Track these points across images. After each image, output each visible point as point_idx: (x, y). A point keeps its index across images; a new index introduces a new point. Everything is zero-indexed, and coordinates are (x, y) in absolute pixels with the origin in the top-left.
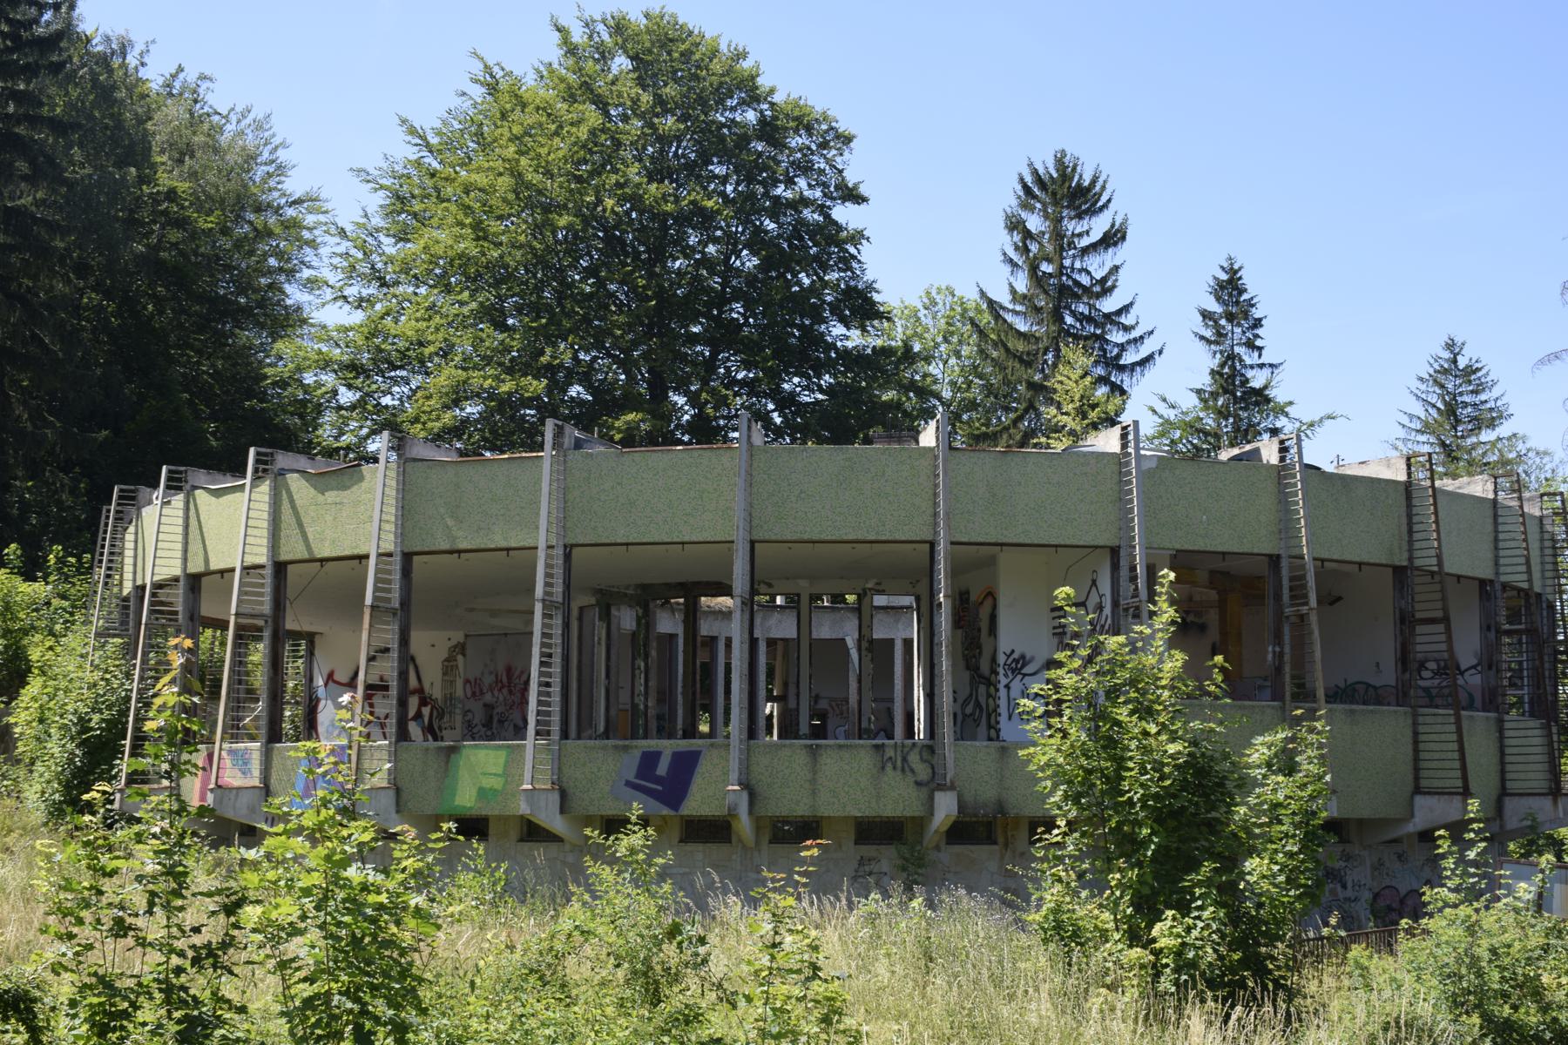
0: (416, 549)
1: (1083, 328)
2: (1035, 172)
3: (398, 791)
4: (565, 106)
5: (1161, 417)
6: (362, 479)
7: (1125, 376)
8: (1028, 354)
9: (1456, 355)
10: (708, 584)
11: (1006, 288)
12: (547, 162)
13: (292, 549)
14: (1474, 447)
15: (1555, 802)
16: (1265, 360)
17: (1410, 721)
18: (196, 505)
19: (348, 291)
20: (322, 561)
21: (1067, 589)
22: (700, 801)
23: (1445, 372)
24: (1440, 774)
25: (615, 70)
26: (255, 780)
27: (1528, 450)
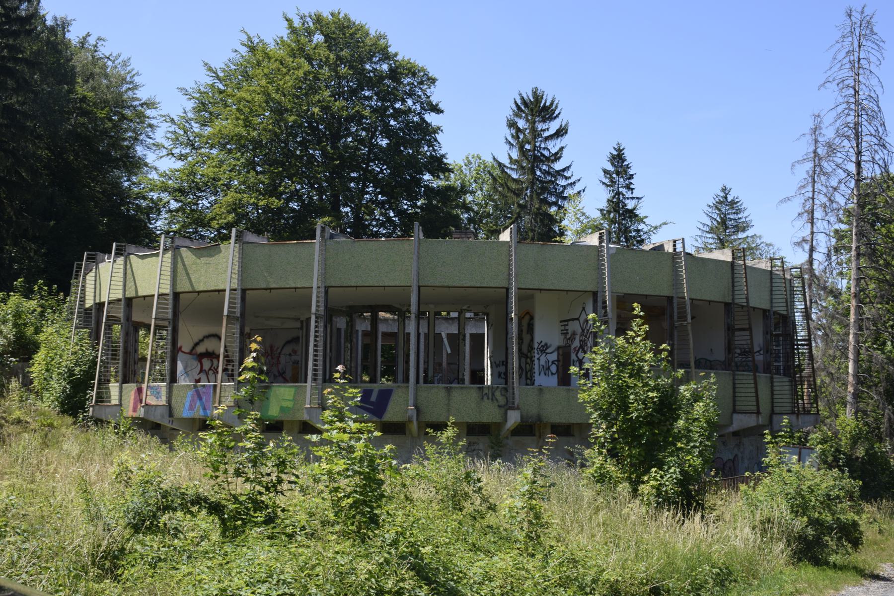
0: (249, 287)
1: (546, 178)
2: (522, 98)
4: (291, 60)
6: (220, 251)
8: (518, 190)
9: (726, 194)
11: (507, 157)
12: (283, 88)
13: (183, 286)
14: (735, 240)
15: (758, 417)
16: (634, 195)
17: (731, 378)
18: (130, 263)
19: (175, 151)
20: (199, 292)
22: (392, 414)
23: (721, 203)
24: (745, 403)
25: (315, 41)
26: (163, 401)
27: (762, 243)
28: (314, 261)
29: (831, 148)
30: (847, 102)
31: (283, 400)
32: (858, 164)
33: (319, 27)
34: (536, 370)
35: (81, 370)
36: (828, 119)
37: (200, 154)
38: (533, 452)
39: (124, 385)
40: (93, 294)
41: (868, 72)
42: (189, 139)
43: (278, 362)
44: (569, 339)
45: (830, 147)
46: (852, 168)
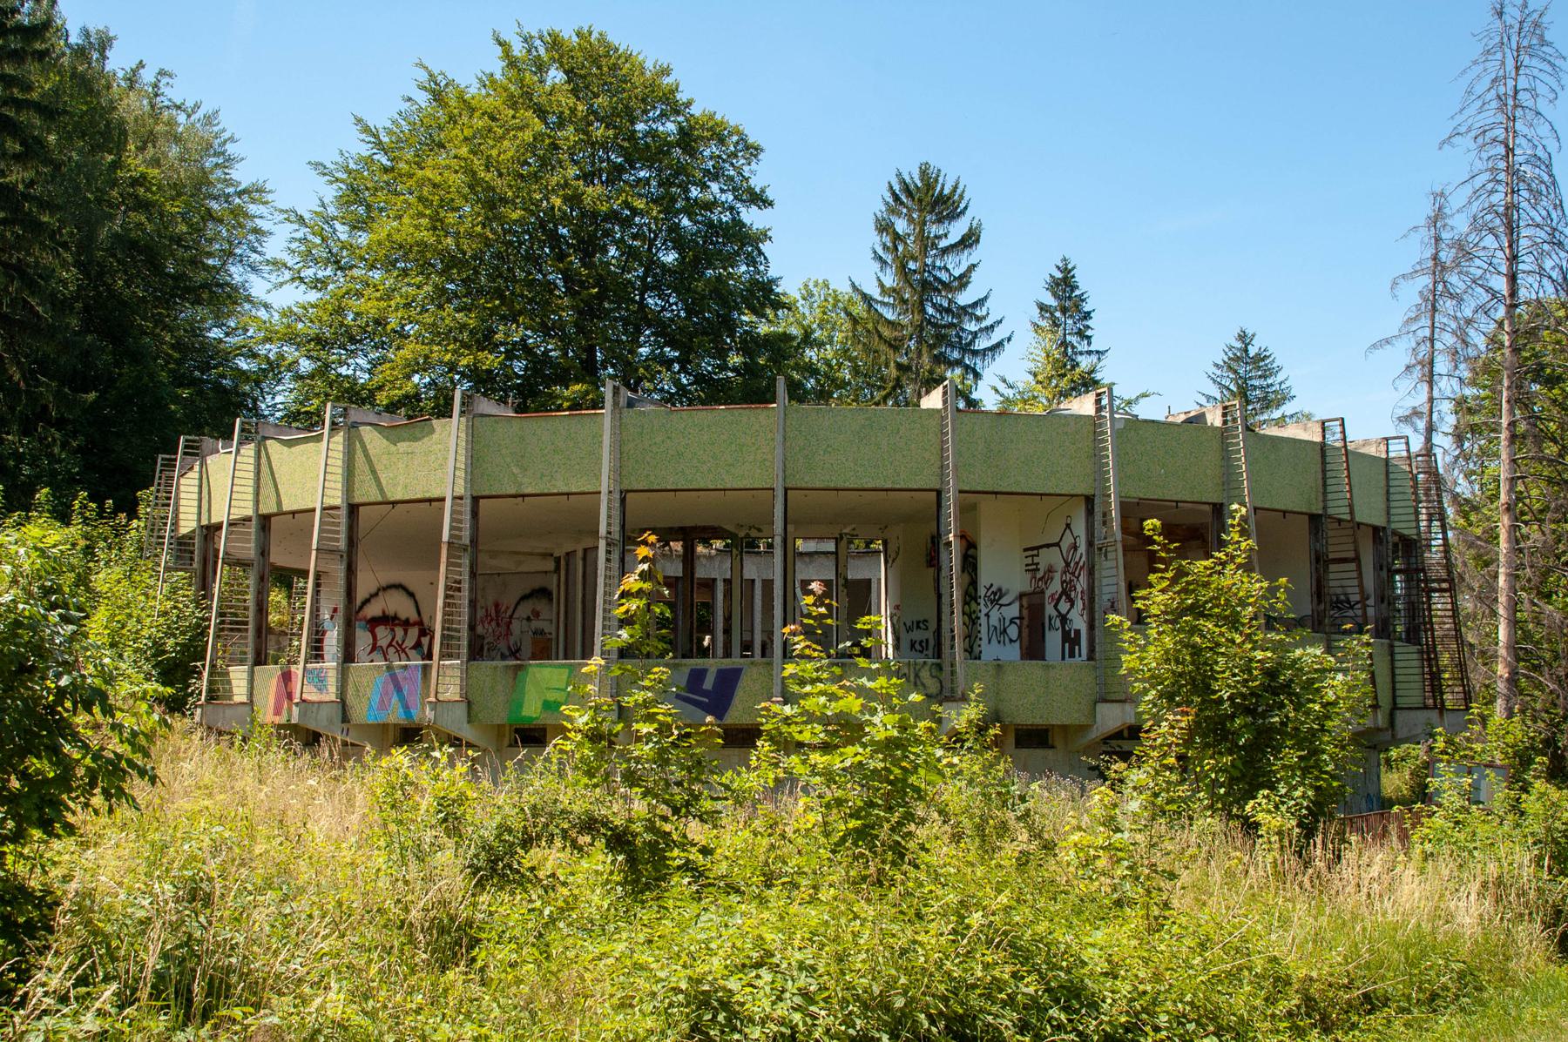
0: (484, 494)
2: (903, 182)
3: (469, 703)
4: (511, 112)
5: (1002, 395)
6: (432, 431)
8: (895, 340)
10: (704, 529)
13: (366, 492)
16: (1092, 348)
18: (267, 454)
20: (394, 503)
21: (1155, 521)
23: (1237, 359)
26: (331, 694)
28: (601, 447)
29: (1464, 251)
30: (1493, 170)
31: (548, 689)
32: (1512, 278)
33: (556, 56)
35: (177, 644)
36: (1457, 200)
37: (353, 278)
39: (257, 668)
40: (195, 510)
41: (1530, 115)
42: (330, 252)
43: (509, 632)
44: (1040, 579)
45: (1461, 248)
46: (1501, 284)
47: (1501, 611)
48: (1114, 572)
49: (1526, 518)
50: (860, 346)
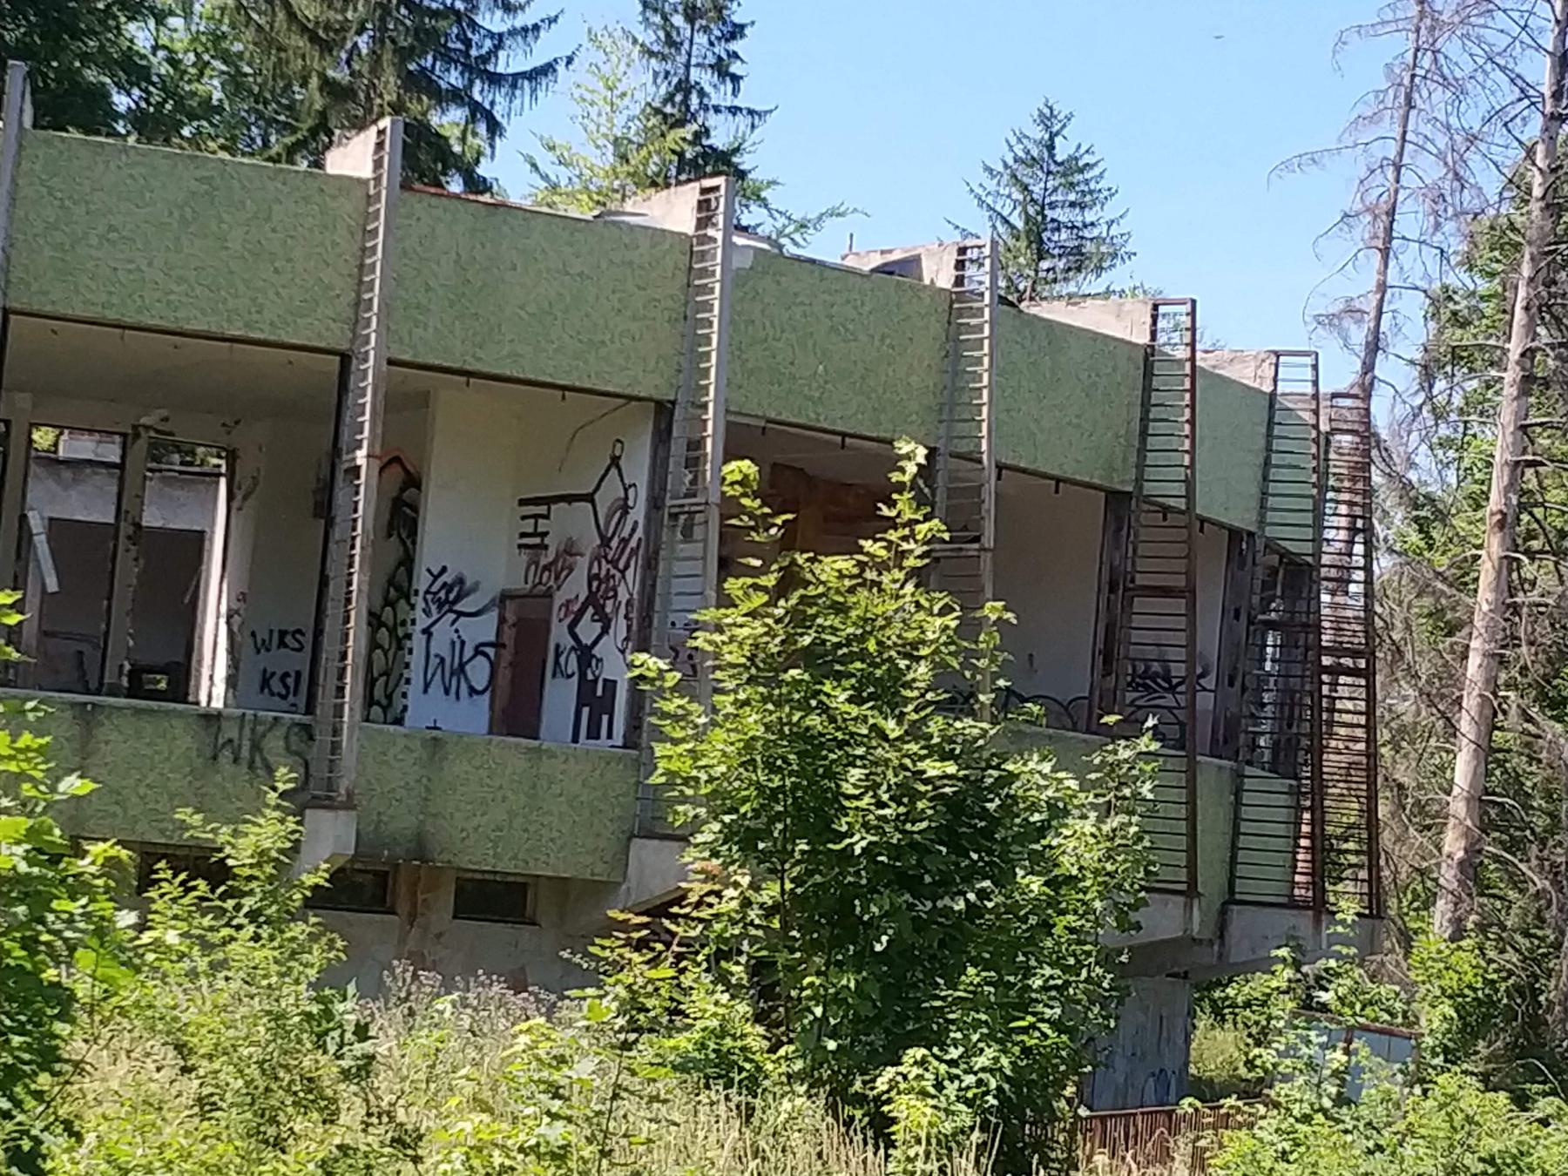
5: (545, 178)
7: (500, 99)
8: (327, 27)
15: (1188, 907)
34: (416, 673)
38: (624, 926)
44: (546, 568)
47: (1465, 725)
48: (695, 567)
49: (1535, 545)
50: (249, 34)
